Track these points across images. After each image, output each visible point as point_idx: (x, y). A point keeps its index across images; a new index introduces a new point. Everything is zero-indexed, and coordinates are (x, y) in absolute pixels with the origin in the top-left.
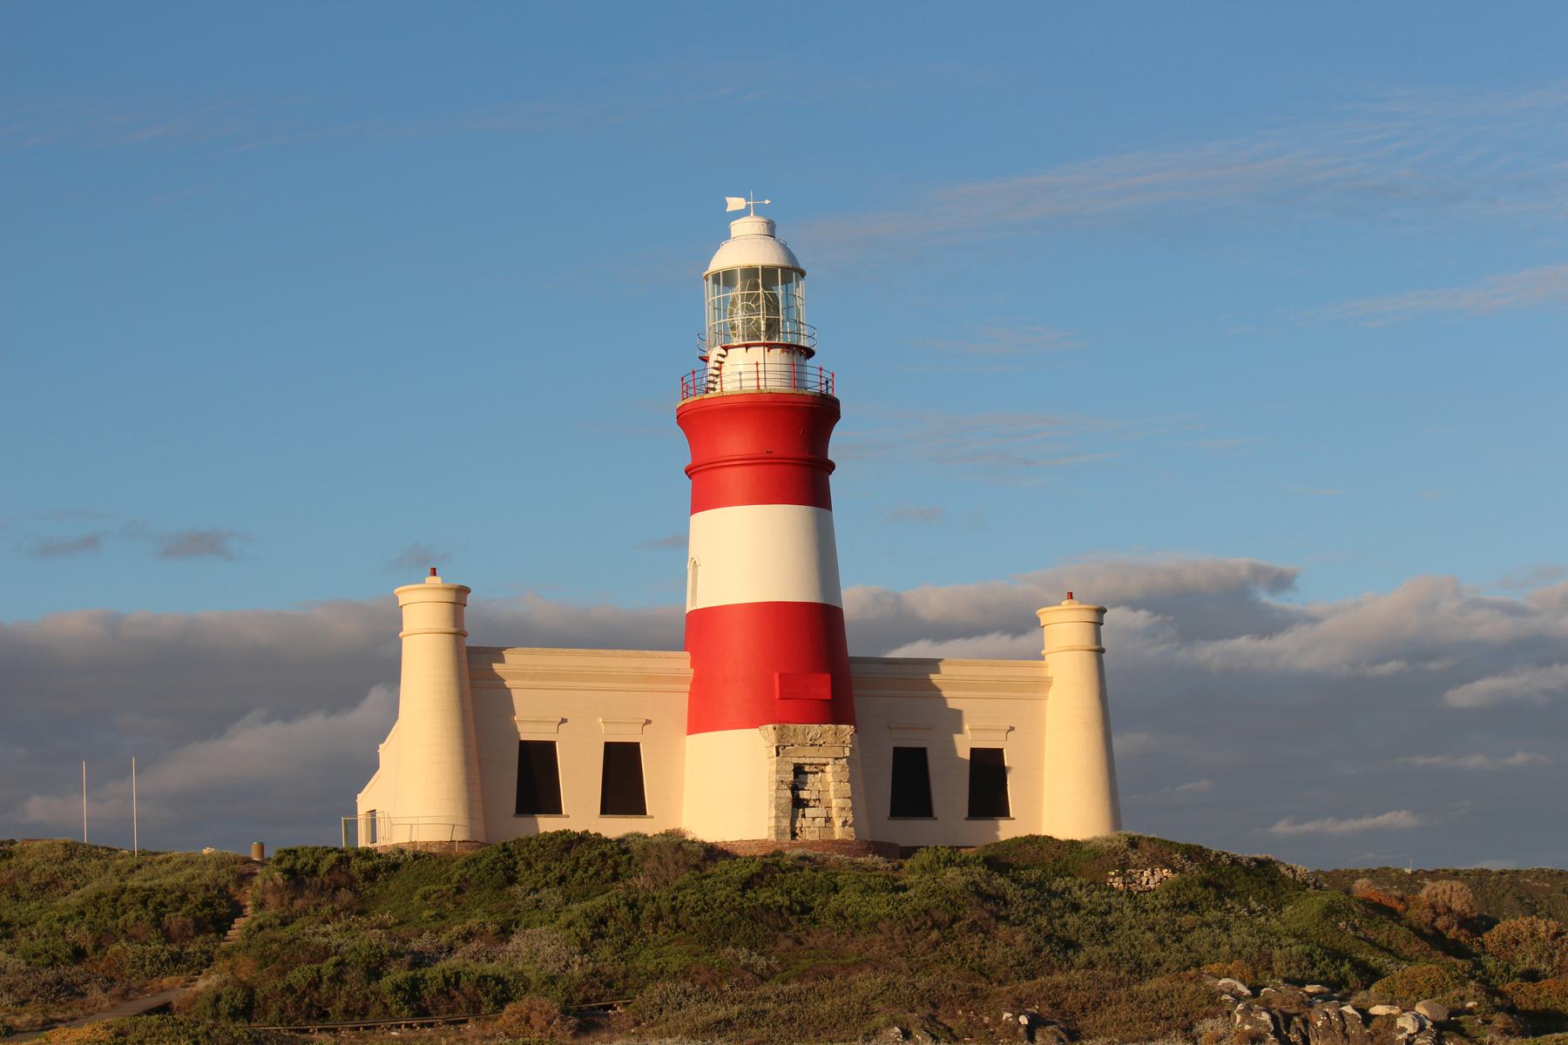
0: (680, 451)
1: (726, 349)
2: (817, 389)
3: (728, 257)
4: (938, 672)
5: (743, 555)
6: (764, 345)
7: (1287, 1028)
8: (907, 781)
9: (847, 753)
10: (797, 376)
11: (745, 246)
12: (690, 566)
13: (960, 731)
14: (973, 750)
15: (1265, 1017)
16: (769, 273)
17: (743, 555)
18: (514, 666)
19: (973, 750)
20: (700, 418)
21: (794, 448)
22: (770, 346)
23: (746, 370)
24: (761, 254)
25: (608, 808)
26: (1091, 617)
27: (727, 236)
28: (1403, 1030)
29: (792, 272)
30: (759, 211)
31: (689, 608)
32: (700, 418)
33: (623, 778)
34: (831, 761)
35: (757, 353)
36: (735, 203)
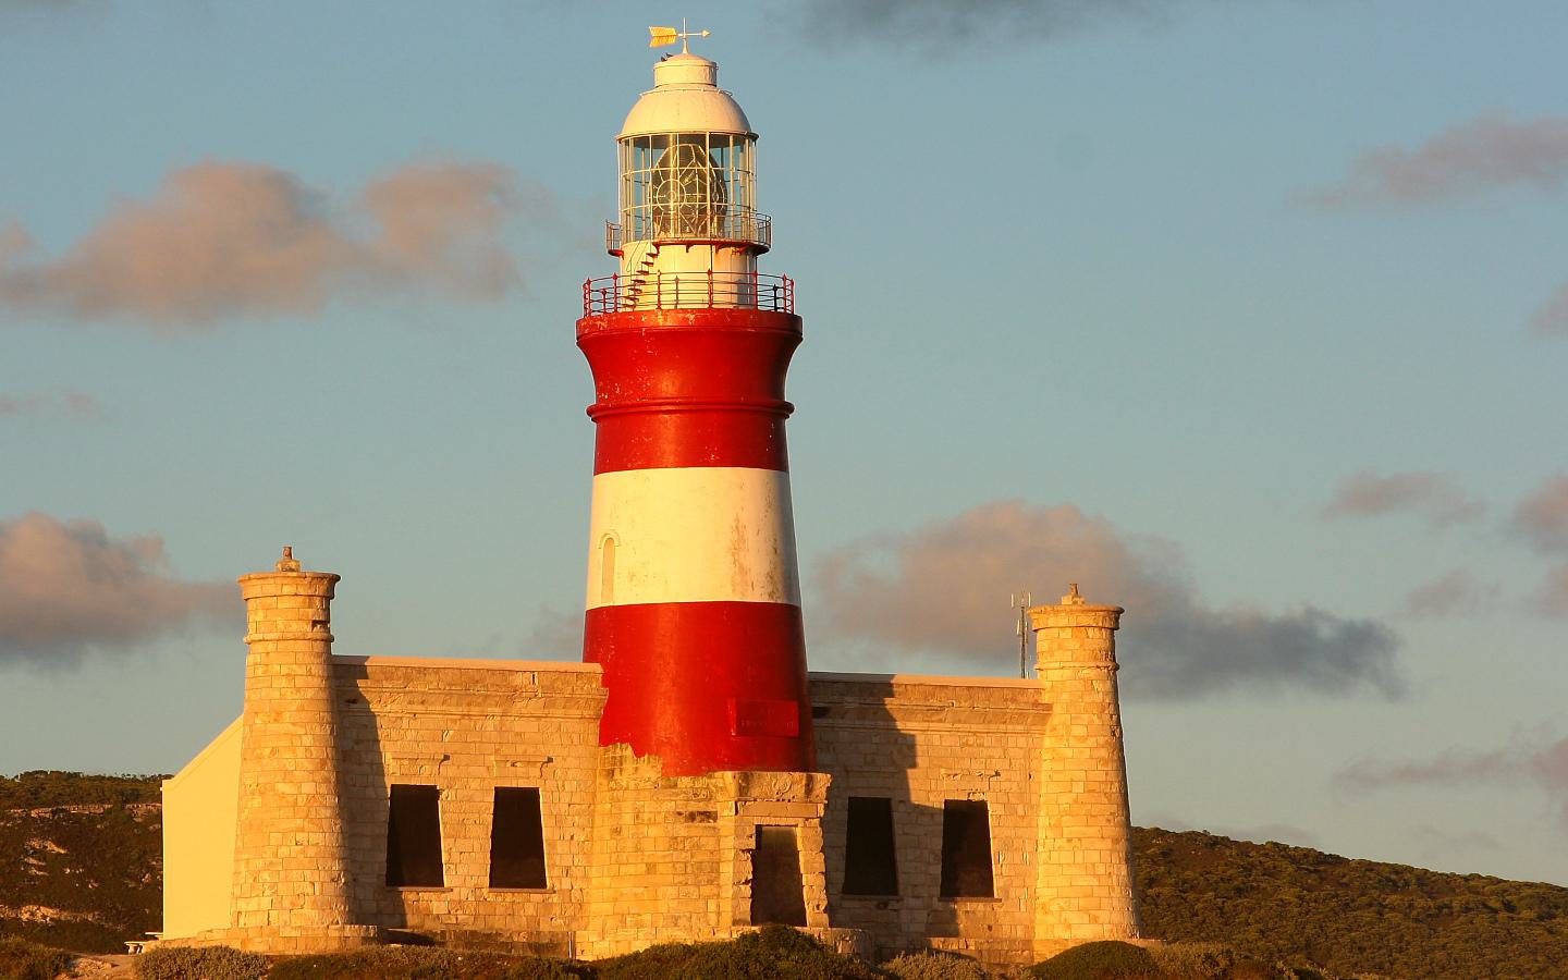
0: (580, 384)
1: (657, 245)
3: (648, 118)
4: (891, 695)
5: (674, 535)
6: (711, 243)
8: (867, 834)
11: (677, 102)
13: (914, 766)
16: (719, 140)
17: (674, 535)
18: (385, 707)
20: (613, 346)
21: (720, 386)
22: (720, 245)
23: (681, 279)
24: (708, 117)
25: (498, 879)
26: (1097, 639)
27: (649, 83)
29: (745, 137)
31: (596, 601)
32: (613, 346)
33: (517, 837)
34: (800, 822)
35: (702, 254)
36: (661, 34)
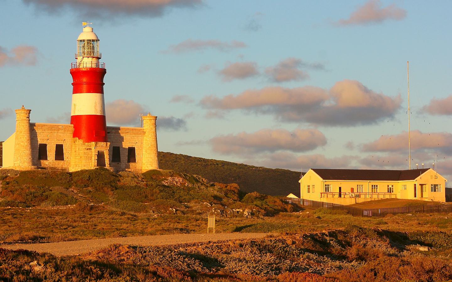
0: (70, 79)
2: (101, 67)
5: (86, 104)
7: (223, 213)
8: (116, 153)
9: (108, 149)
10: (97, 64)
12: (73, 105)
13: (123, 141)
14: (129, 147)
15: (219, 211)
16: (93, 41)
19: (129, 147)
21: (92, 80)
23: (87, 63)
24: (92, 37)
25: (57, 158)
28: (245, 215)
30: (90, 26)
31: (73, 114)
32: (76, 73)
33: (60, 153)
34: (105, 150)
